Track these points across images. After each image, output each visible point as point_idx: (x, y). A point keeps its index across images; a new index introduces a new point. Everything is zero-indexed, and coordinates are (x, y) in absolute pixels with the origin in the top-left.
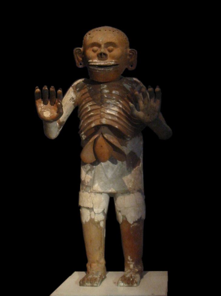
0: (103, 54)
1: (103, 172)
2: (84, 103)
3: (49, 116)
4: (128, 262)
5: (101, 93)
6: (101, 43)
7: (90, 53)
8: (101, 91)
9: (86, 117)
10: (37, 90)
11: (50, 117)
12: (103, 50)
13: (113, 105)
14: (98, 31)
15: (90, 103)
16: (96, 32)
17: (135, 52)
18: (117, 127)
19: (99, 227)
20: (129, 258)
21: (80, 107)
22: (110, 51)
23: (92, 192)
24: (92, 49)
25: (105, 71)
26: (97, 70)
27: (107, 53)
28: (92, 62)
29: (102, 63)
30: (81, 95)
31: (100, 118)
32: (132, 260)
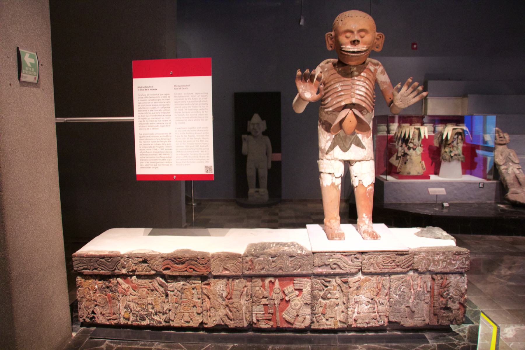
2: (332, 83)
3: (310, 97)
4: (363, 219)
7: (343, 39)
9: (335, 96)
10: (298, 73)
12: (357, 37)
15: (341, 83)
17: (382, 36)
20: (364, 215)
22: (362, 37)
24: (344, 35)
27: (359, 39)
28: (345, 48)
29: (355, 50)
31: (350, 97)
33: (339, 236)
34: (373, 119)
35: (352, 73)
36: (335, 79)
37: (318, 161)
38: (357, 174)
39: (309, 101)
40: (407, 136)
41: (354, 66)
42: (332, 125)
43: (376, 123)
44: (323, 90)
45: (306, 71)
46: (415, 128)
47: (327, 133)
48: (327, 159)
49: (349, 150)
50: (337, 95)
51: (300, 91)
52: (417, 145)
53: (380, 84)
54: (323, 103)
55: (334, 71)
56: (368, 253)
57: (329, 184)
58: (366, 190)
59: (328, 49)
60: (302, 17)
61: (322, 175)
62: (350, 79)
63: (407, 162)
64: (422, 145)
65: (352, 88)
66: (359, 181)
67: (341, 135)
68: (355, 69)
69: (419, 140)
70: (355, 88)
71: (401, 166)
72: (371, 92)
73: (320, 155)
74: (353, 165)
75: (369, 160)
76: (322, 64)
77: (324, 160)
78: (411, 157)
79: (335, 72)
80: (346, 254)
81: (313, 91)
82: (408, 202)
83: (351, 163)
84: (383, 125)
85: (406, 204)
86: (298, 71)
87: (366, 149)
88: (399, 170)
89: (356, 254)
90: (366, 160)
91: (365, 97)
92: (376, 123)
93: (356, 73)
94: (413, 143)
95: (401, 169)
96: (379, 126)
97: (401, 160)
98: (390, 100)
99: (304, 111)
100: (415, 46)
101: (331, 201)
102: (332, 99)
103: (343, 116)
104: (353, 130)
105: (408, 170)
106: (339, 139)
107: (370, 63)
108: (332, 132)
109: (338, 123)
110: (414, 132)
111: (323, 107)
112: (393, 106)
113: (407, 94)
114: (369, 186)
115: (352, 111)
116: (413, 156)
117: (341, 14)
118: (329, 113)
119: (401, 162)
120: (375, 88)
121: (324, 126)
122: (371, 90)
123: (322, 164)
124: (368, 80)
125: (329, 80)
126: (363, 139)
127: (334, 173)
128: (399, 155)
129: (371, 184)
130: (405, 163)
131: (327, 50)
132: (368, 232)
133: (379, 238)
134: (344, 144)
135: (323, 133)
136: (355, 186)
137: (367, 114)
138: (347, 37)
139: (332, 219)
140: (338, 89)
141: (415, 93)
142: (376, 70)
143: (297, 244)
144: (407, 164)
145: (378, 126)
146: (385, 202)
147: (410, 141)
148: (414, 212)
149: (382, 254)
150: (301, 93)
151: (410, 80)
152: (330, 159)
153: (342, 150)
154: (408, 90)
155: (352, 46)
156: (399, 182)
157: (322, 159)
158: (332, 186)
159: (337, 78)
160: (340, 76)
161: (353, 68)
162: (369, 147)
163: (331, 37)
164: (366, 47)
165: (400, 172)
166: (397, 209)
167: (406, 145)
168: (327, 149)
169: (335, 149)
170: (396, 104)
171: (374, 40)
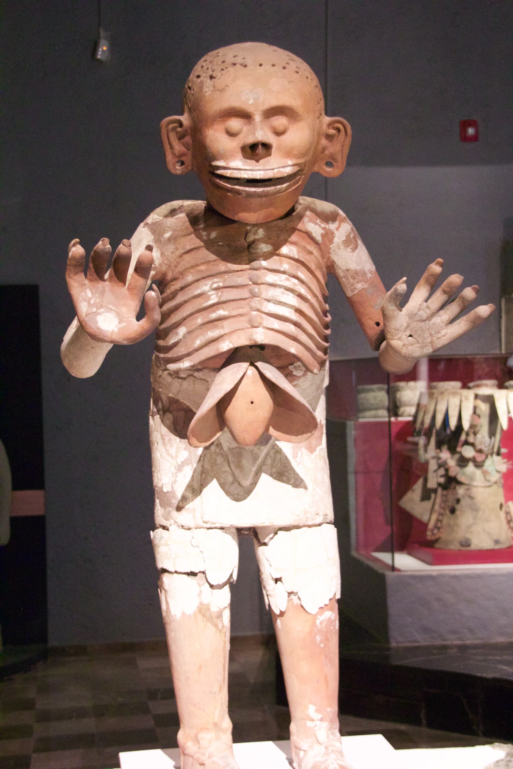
1: (227, 468)
3: (116, 330)
6: (250, 109)
9: (200, 321)
10: (73, 249)
15: (216, 280)
18: (293, 351)
19: (220, 626)
20: (311, 710)
22: (278, 133)
27: (270, 138)
29: (259, 175)
30: (178, 253)
32: (320, 716)
34: (328, 388)
35: (251, 245)
36: (197, 265)
37: (151, 533)
39: (111, 342)
40: (453, 423)
41: (257, 225)
42: (195, 414)
43: (354, 384)
44: (158, 307)
45: (100, 243)
46: (476, 396)
47: (178, 439)
50: (206, 320)
51: (83, 308)
52: (485, 449)
54: (161, 343)
55: (193, 241)
57: (191, 609)
58: (314, 624)
59: (173, 171)
60: (102, 33)
61: (166, 578)
62: (248, 266)
63: (458, 507)
64: (503, 450)
65: (254, 295)
67: (225, 446)
68: (261, 232)
69: (492, 434)
70: (264, 296)
71: (438, 520)
72: (316, 305)
73: (159, 512)
74: (266, 541)
75: (320, 525)
76: (154, 217)
78: (468, 489)
79: (198, 243)
81: (124, 310)
82: (469, 642)
83: (260, 536)
84: (375, 387)
85: (463, 648)
86: (74, 245)
87: (306, 488)
88: (433, 534)
90: (310, 523)
91: (296, 324)
92: (354, 384)
93: (265, 248)
94: (473, 445)
95: (439, 529)
96: (363, 391)
97: (438, 500)
98: (378, 329)
99: (99, 370)
100: (471, 131)
101: (200, 667)
102: (189, 333)
103: (228, 387)
104: (260, 431)
105: (460, 534)
106: (220, 460)
107: (308, 213)
108: (194, 441)
109: (211, 410)
110: (475, 408)
111: (162, 355)
112: (386, 347)
113: (429, 312)
115: (257, 368)
116: (476, 487)
117: (209, 57)
118: (182, 375)
119: (437, 507)
120: (327, 293)
121: (169, 416)
122: (313, 300)
123: (163, 541)
125: (180, 269)
126: (295, 456)
127: (204, 573)
128: (432, 484)
130: (453, 511)
131: (169, 172)
134: (234, 475)
135: (167, 438)
136: (277, 612)
137: (304, 375)
138: (231, 134)
140: (209, 298)
141: (454, 308)
142: (328, 236)
144: (458, 513)
145: (360, 392)
146: (393, 644)
147: (463, 437)
148: (490, 675)
150: (87, 315)
151: (435, 268)
152: (192, 525)
153: (228, 493)
154: (430, 301)
155: (248, 161)
156: (435, 573)
157: (164, 528)
158: (200, 617)
159: (203, 263)
161: (253, 230)
163: (179, 129)
165: (437, 540)
166: (434, 667)
167: (453, 450)
168: (180, 491)
169: (205, 491)
170: (395, 343)
171: (319, 139)
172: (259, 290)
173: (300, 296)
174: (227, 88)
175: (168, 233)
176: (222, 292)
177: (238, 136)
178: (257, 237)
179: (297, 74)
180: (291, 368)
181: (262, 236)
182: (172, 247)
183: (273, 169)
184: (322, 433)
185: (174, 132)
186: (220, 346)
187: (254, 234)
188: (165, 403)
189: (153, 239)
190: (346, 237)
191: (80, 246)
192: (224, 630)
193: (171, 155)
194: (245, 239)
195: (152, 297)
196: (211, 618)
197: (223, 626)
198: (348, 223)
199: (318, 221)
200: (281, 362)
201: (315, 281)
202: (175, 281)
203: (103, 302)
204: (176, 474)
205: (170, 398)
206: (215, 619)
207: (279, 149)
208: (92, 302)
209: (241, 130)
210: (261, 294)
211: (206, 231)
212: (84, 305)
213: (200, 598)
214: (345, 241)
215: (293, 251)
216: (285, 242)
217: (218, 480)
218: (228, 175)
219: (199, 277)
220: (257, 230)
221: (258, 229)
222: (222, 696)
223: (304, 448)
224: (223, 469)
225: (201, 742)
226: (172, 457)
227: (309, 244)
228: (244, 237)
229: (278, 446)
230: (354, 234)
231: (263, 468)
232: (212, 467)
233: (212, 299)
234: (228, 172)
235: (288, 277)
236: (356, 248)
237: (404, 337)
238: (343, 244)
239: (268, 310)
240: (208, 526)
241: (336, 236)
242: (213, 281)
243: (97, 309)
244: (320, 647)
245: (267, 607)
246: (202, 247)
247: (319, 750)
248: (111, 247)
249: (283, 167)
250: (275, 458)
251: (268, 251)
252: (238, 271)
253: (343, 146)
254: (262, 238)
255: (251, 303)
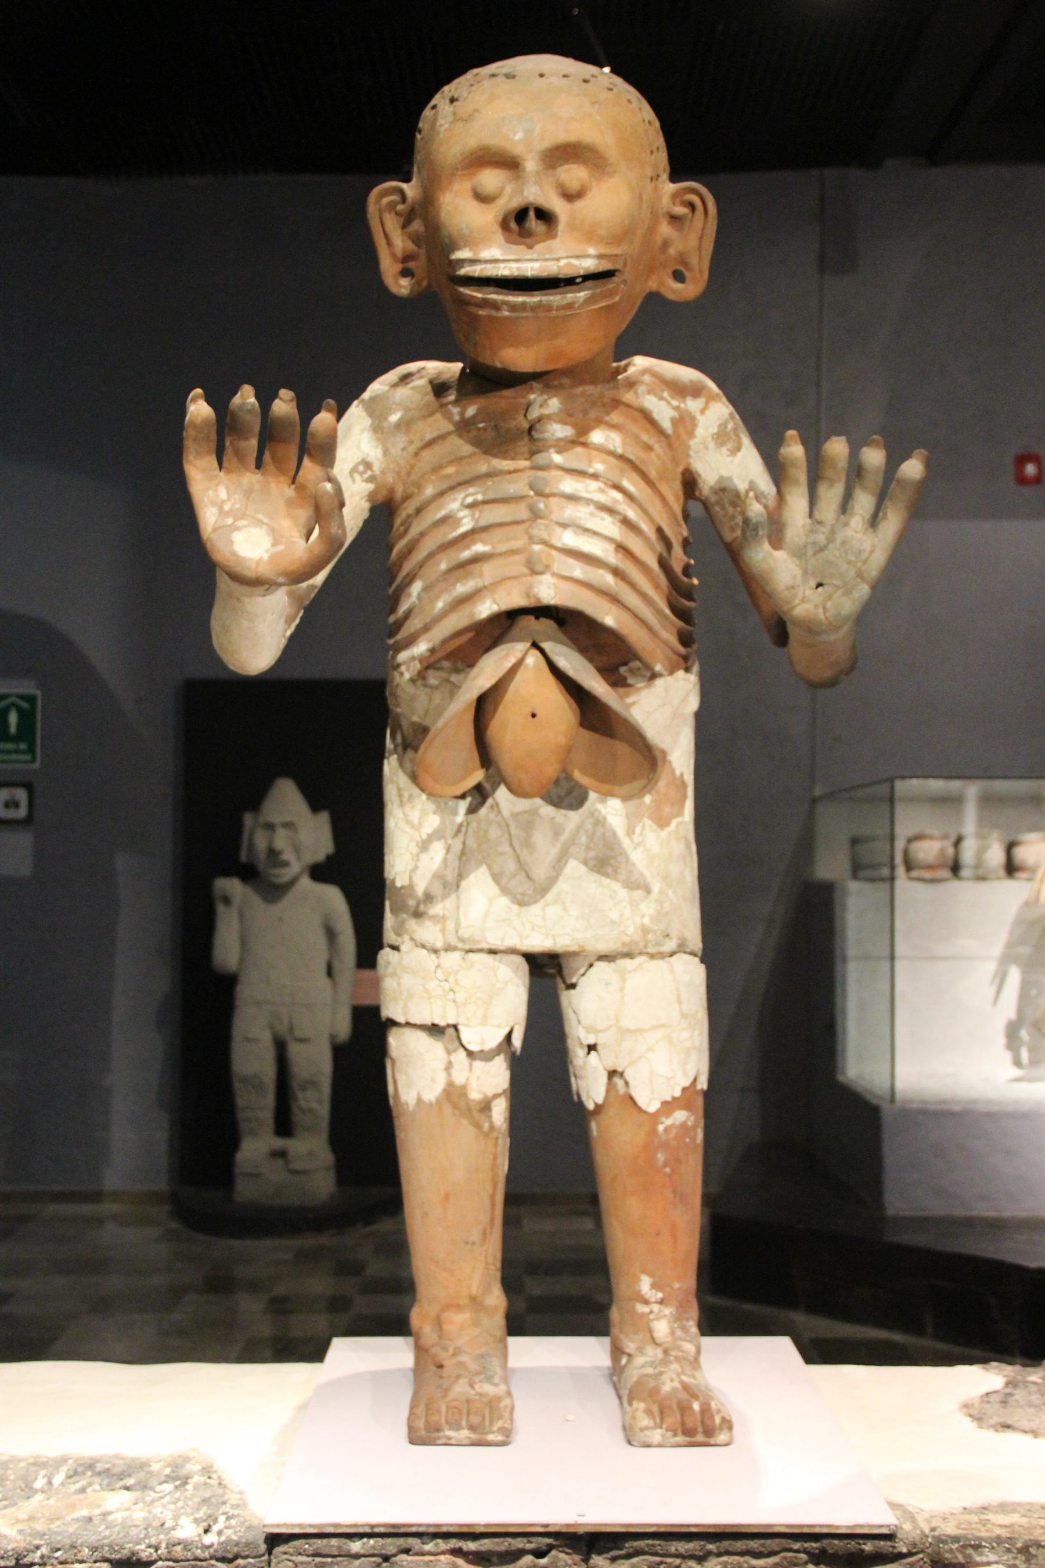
0: (532, 214)
1: (506, 848)
3: (266, 557)
5: (532, 439)
6: (518, 150)
8: (531, 429)
9: (443, 566)
11: (271, 557)
13: (592, 508)
14: (499, 79)
15: (471, 490)
16: (487, 84)
18: (609, 621)
19: (486, 1126)
20: (645, 1285)
21: (409, 508)
22: (570, 196)
23: (455, 949)
25: (548, 308)
26: (504, 303)
28: (473, 262)
29: (531, 268)
30: (412, 449)
31: (526, 571)
32: (660, 1295)
33: (475, 1420)
38: (597, 1031)
48: (423, 946)
49: (550, 897)
50: (454, 563)
53: (717, 508)
56: (630, 1545)
57: (432, 1093)
58: (654, 1130)
59: (394, 289)
61: (395, 1040)
65: (536, 515)
66: (612, 1074)
70: (555, 516)
74: (574, 980)
75: (672, 954)
76: (377, 387)
77: (403, 948)
80: (485, 1544)
86: (194, 400)
89: (550, 1548)
90: (651, 950)
91: (616, 572)
93: (559, 431)
101: (447, 1197)
102: (426, 589)
114: (668, 1107)
123: (390, 970)
124: (634, 476)
126: (630, 832)
127: (455, 1027)
129: (677, 1093)
132: (654, 1392)
133: (722, 1437)
135: (406, 794)
138: (483, 198)
139: (453, 1306)
140: (458, 522)
142: (685, 422)
143: (207, 1471)
149: (719, 1555)
150: (215, 530)
152: (439, 944)
155: (514, 247)
157: (395, 948)
158: (448, 1109)
159: (450, 463)
160: (467, 449)
162: (666, 878)
164: (600, 257)
172: (546, 506)
173: (626, 522)
174: (477, 114)
175: (396, 413)
176: (481, 512)
177: (496, 201)
178: (546, 411)
179: (610, 92)
180: (623, 670)
181: (556, 411)
182: (404, 439)
183: (558, 260)
184: (684, 797)
185: (393, 213)
186: (475, 610)
187: (541, 406)
188: (406, 733)
189: (371, 425)
190: (719, 426)
191: (205, 404)
192: (495, 1134)
193: (388, 257)
194: (525, 416)
195: (327, 492)
196: (469, 1110)
197: (492, 1128)
198: (723, 403)
199: (666, 394)
200: (605, 659)
201: (658, 503)
202: (408, 501)
203: (246, 509)
204: (417, 855)
205: (414, 723)
206: (475, 1114)
207: (572, 226)
208: (227, 508)
209: (501, 190)
210: (551, 513)
211: (458, 406)
212: (211, 512)
213: (449, 1074)
214: (717, 434)
215: (613, 440)
216: (599, 422)
217: (489, 867)
218: (476, 274)
219: (445, 486)
220: (546, 401)
221: (550, 398)
222: (486, 1250)
223: (649, 817)
224: (500, 849)
225: (445, 1327)
226: (413, 827)
227: (647, 431)
228: (524, 412)
229: (600, 813)
230: (735, 424)
231: (571, 850)
232: (479, 845)
233: (465, 524)
234: (476, 270)
235: (602, 486)
236: (738, 449)
237: (809, 593)
238: (712, 441)
239: (564, 544)
240: (467, 947)
241: (700, 424)
242: (467, 492)
243: (235, 520)
244: (665, 1174)
245: (575, 1098)
246: (449, 433)
247: (653, 1353)
248: (257, 404)
249: (578, 257)
250: (593, 834)
251: (566, 437)
252: (510, 472)
253: (701, 238)
254: (554, 414)
255: (530, 530)
